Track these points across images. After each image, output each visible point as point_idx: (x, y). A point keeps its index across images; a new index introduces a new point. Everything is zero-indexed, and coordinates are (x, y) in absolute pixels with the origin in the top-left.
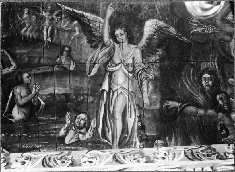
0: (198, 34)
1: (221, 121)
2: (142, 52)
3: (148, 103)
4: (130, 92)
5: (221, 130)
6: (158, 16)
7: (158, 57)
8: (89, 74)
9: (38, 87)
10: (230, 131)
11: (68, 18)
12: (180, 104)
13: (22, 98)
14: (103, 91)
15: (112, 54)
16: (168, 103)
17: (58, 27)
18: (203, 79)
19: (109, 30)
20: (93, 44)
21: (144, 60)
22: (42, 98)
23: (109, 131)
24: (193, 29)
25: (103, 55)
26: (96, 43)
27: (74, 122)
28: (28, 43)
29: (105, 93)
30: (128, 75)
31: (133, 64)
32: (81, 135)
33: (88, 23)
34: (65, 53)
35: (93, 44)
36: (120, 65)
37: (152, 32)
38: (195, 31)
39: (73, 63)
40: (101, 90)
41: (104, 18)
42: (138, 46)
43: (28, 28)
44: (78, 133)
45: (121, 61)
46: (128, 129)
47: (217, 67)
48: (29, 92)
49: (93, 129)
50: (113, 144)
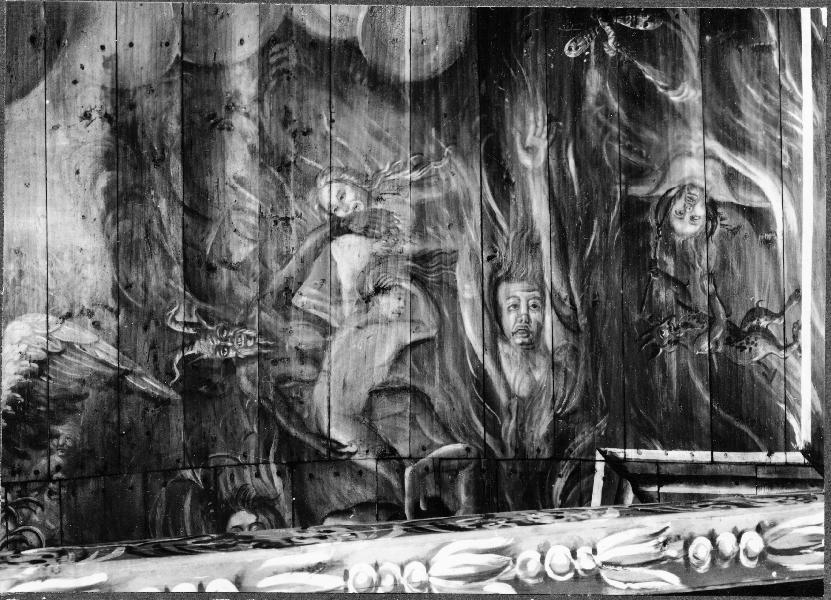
38: (190, 352)
47: (277, 481)
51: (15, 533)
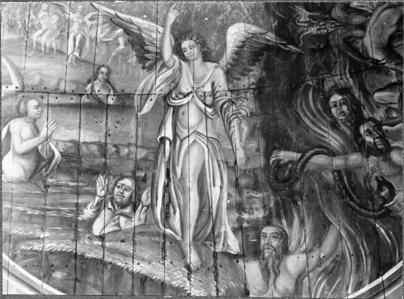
0: (311, 37)
1: (375, 172)
2: (228, 73)
3: (244, 159)
4: (210, 139)
5: (380, 189)
6: (247, 18)
7: (252, 80)
8: (141, 110)
9: (52, 127)
10: (395, 187)
11: (108, 24)
12: (299, 155)
13: (23, 140)
14: (163, 140)
15: (178, 79)
16: (278, 155)
17: (92, 35)
18: (331, 105)
19: (171, 42)
20: (147, 64)
21: (231, 86)
22: (57, 146)
23: (175, 212)
24: (302, 32)
25: (163, 80)
26: (150, 62)
27: (112, 193)
28: (43, 53)
29: (167, 143)
30: (204, 111)
31: (213, 93)
32: (122, 220)
33: (139, 32)
34: (100, 76)
35: (147, 64)
36: (191, 96)
37: (241, 42)
38: (307, 33)
39: (113, 94)
40: (159, 137)
41: (164, 26)
42: (219, 64)
43: (44, 32)
44: (119, 214)
45: (192, 89)
46: (209, 209)
47: (351, 80)
48: (36, 131)
49: (145, 208)
50: (182, 237)
51: (236, 111)
